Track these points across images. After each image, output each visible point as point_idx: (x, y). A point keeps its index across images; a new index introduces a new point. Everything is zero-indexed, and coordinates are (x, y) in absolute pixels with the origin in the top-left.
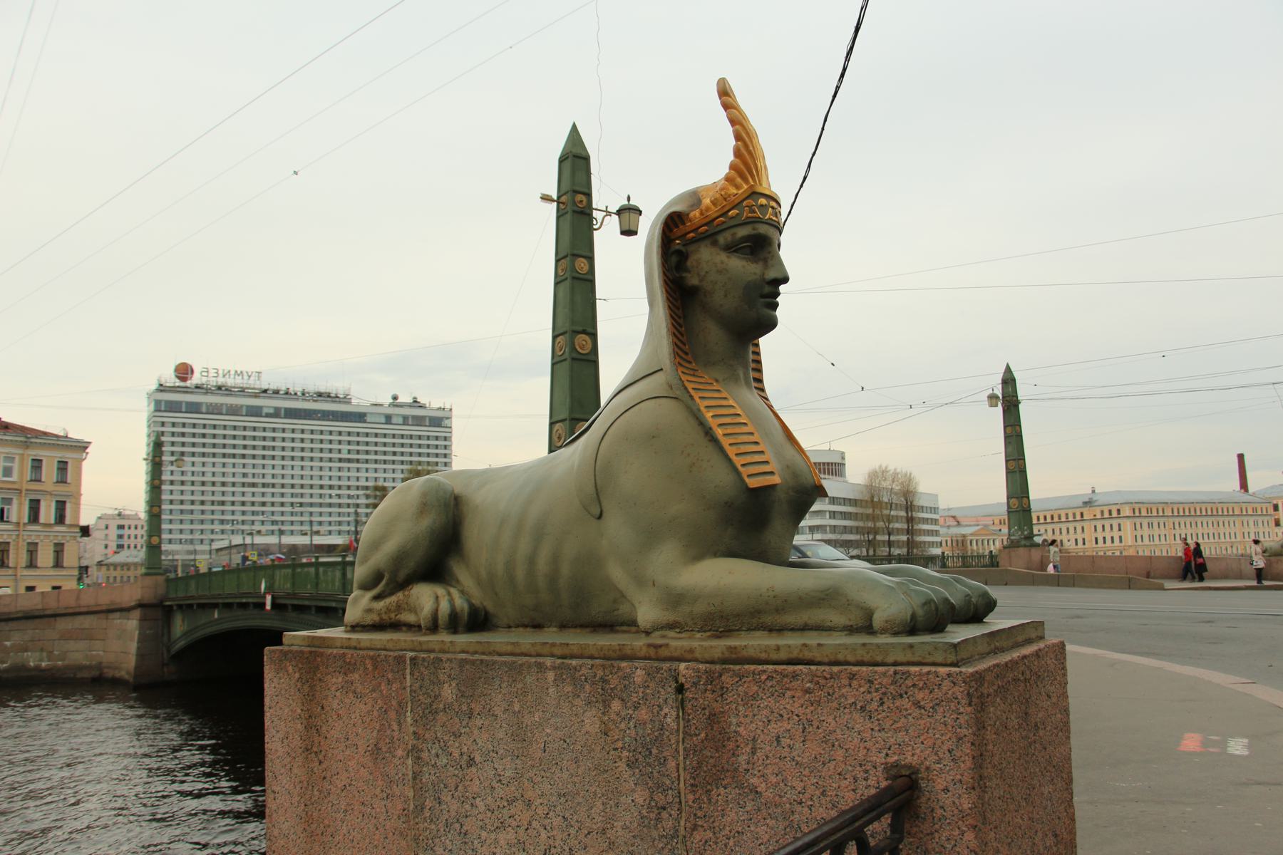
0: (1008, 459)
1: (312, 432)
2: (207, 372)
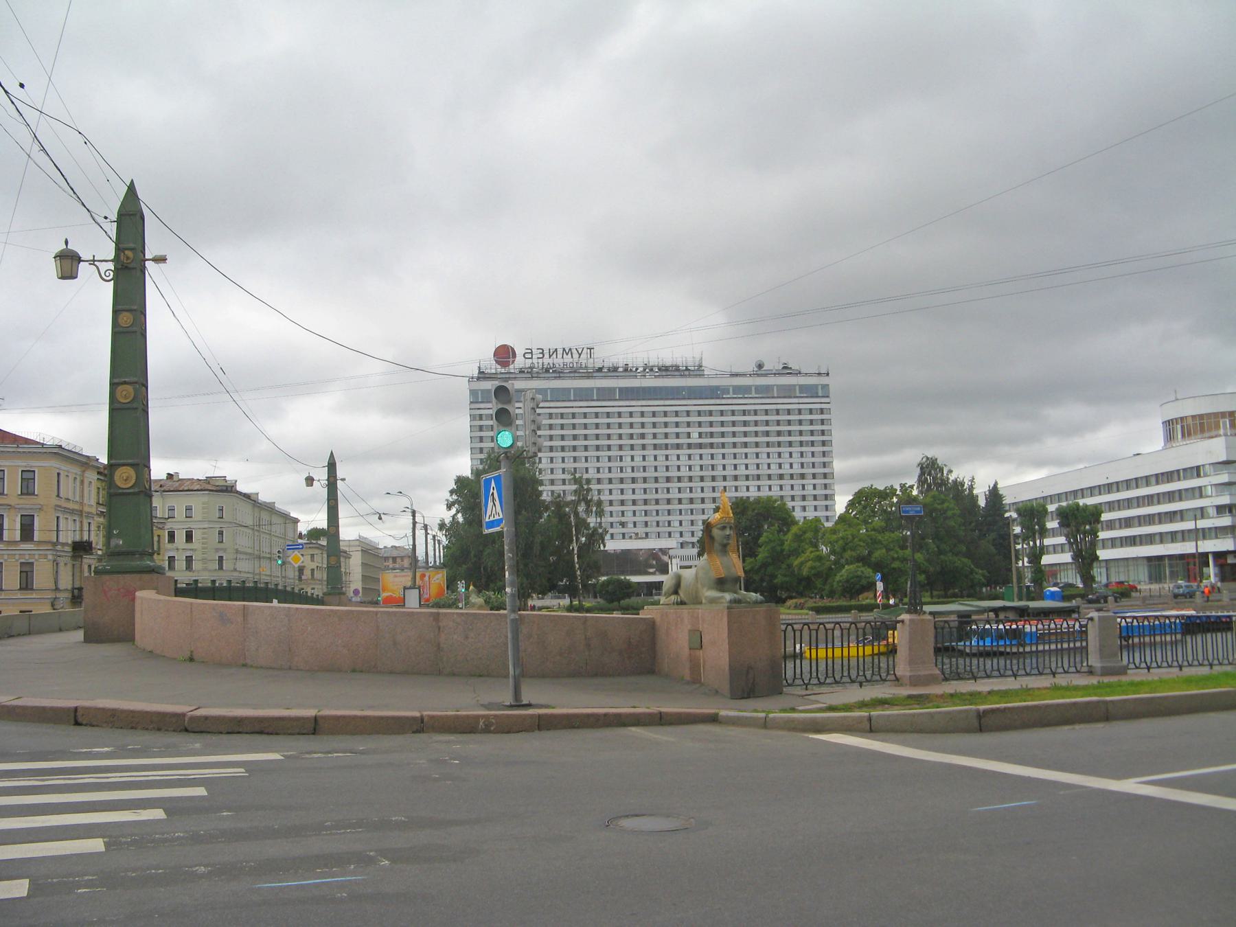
0: (116, 381)
1: (654, 414)
2: (531, 353)
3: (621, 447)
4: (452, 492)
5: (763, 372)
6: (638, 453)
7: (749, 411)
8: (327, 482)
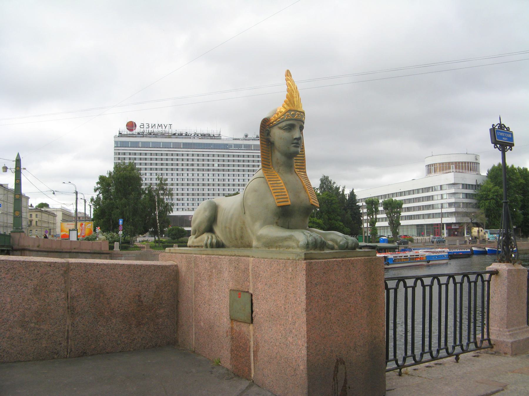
2: (144, 125)
3: (183, 170)
4: (98, 183)
5: (247, 139)
6: (190, 172)
7: (241, 155)
8: (15, 170)
